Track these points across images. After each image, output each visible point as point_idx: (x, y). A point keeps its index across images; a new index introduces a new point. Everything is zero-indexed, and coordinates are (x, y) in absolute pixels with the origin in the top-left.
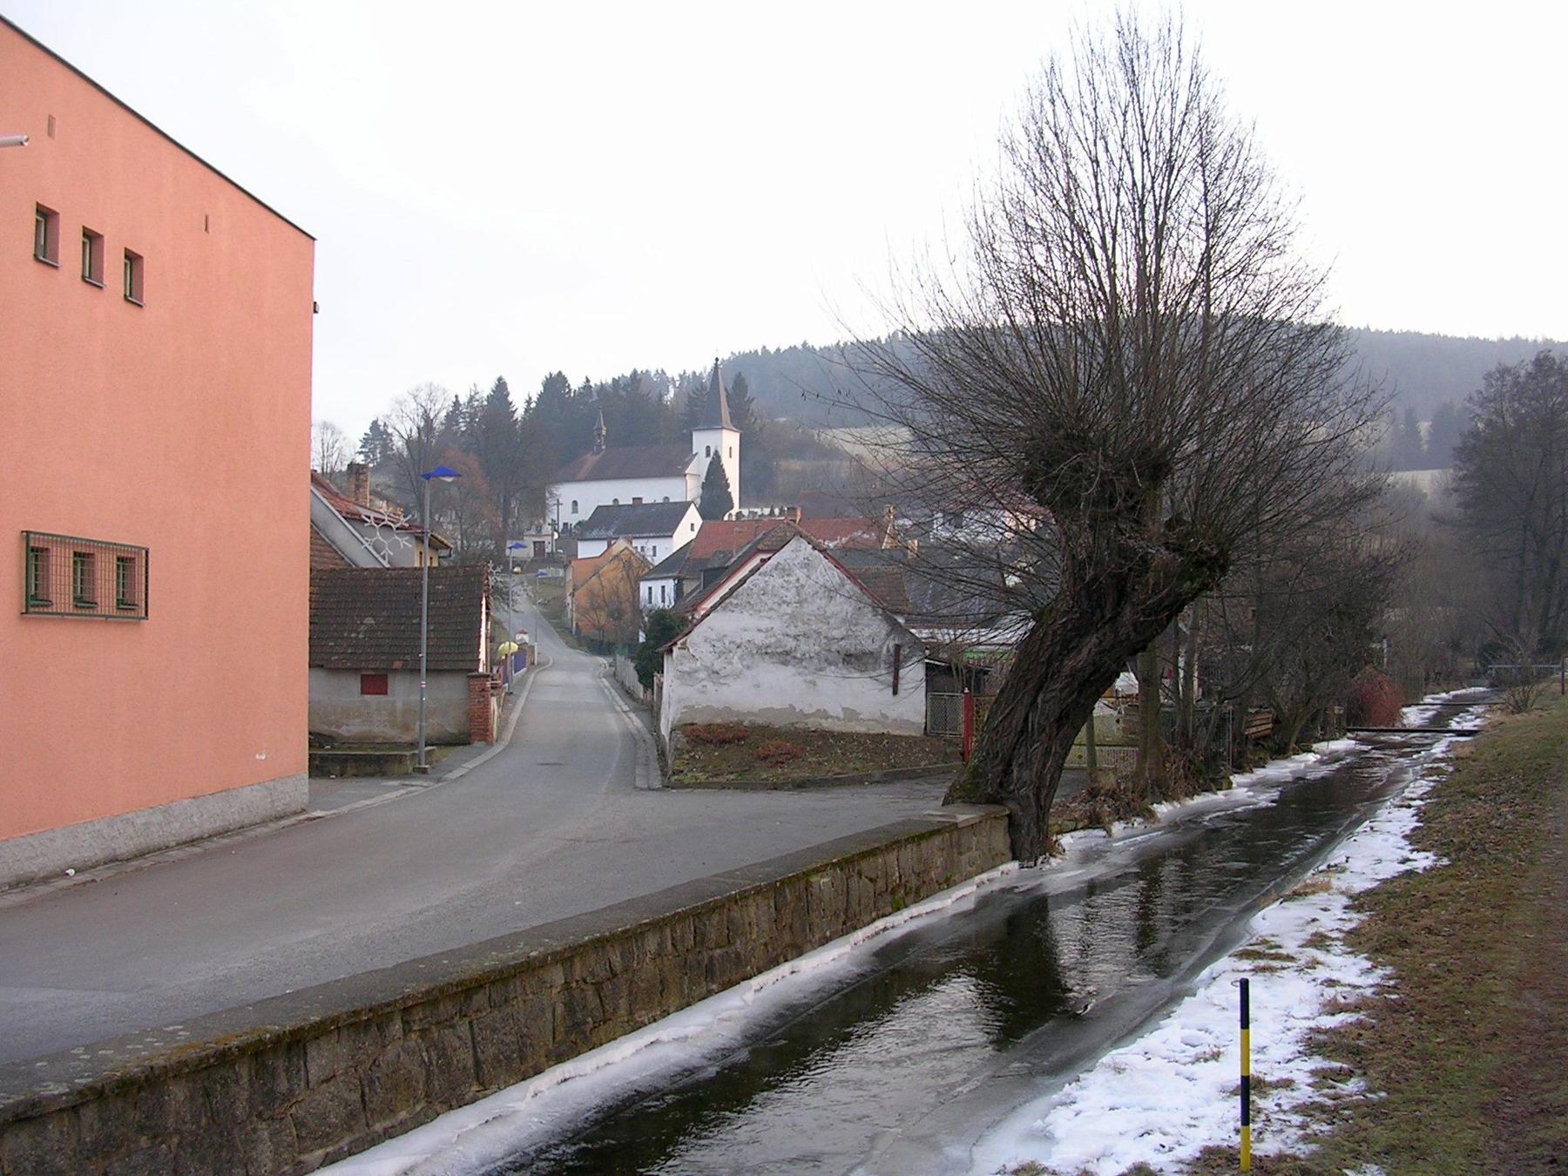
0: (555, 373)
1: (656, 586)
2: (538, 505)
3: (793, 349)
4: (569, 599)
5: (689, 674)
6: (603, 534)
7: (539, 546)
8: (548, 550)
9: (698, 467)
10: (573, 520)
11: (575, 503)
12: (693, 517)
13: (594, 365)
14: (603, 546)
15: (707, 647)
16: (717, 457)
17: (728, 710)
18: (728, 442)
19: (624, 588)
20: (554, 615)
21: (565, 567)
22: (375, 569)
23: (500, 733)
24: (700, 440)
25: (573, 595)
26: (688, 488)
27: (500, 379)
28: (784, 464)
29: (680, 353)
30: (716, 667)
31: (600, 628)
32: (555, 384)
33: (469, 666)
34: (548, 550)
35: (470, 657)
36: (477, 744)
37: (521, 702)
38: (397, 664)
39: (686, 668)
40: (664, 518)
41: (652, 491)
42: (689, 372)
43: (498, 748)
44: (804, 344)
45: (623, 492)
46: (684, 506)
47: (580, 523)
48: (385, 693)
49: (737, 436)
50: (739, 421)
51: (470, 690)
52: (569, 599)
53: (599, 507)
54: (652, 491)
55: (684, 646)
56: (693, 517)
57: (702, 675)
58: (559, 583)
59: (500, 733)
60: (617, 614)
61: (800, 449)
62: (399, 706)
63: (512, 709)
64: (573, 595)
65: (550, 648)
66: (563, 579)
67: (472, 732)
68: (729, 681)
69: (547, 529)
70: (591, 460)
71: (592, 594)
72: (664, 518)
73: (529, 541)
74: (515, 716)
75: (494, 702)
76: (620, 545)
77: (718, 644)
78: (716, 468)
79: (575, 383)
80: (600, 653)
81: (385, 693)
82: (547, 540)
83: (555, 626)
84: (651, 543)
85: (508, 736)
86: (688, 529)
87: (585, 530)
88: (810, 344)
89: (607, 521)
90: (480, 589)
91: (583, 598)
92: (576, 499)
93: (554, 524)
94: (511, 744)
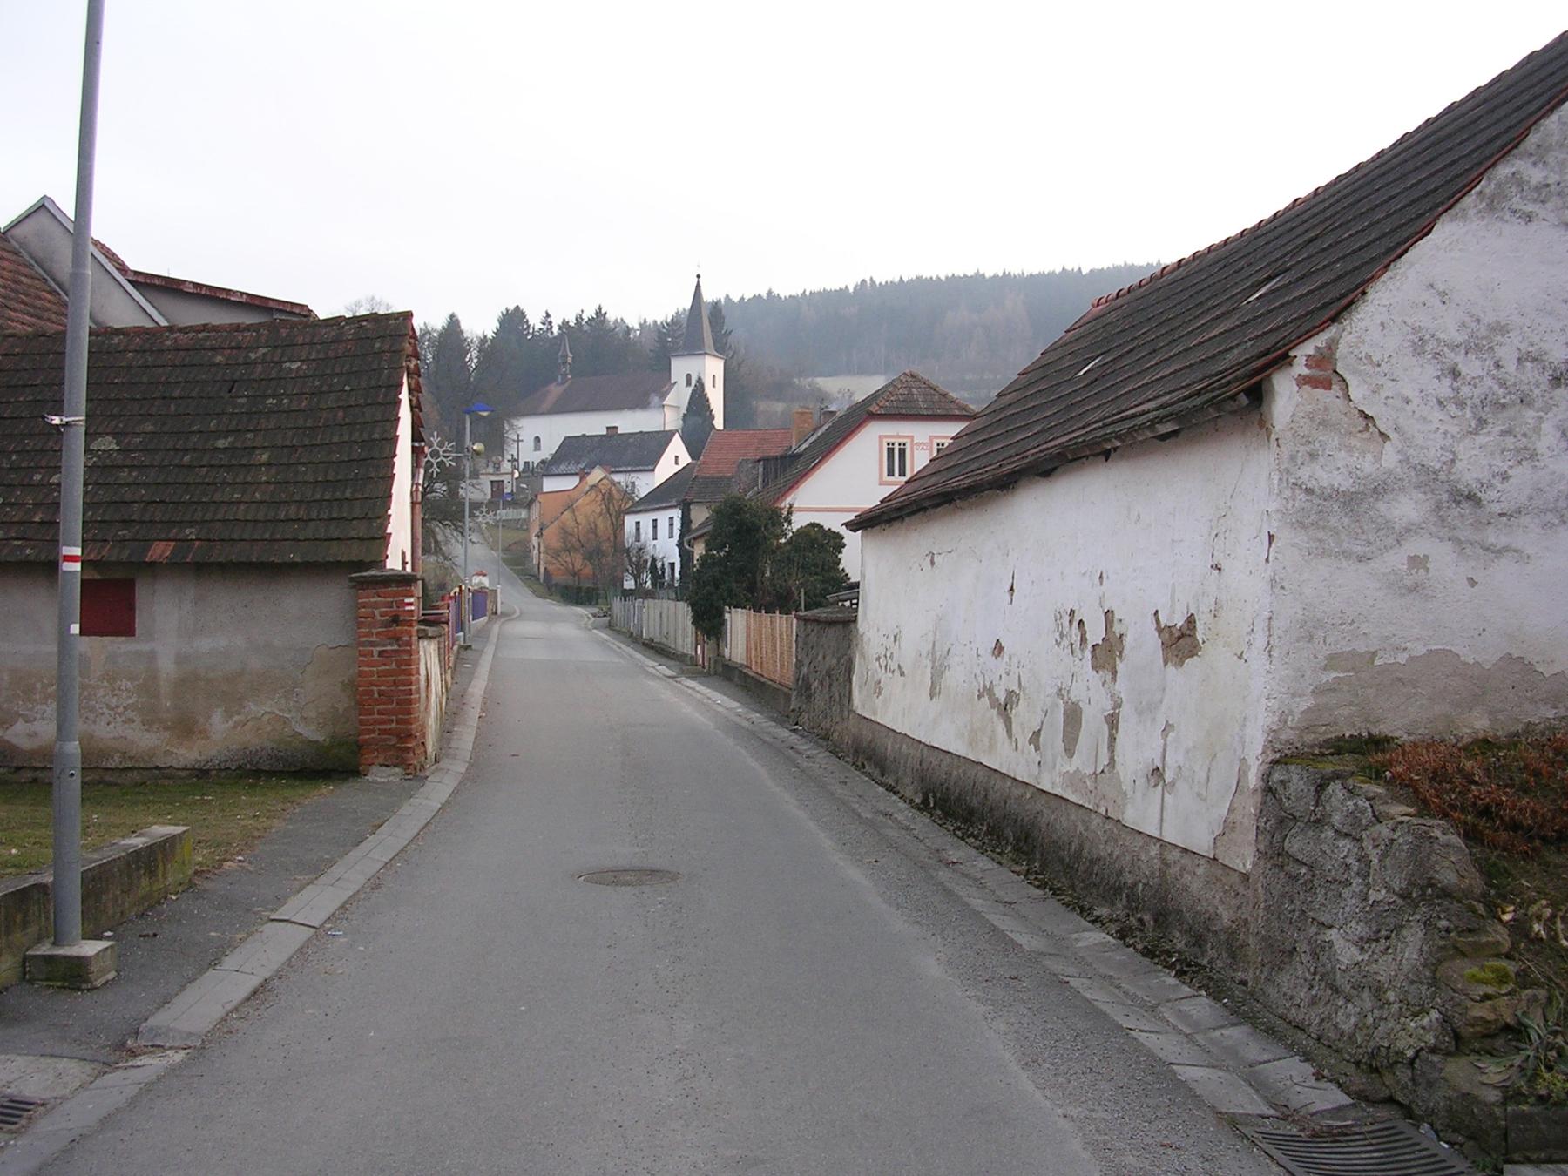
0: (512, 308)
1: (646, 520)
2: (496, 442)
3: (757, 298)
4: (535, 541)
5: (1350, 501)
6: (574, 468)
7: (497, 486)
8: (508, 490)
9: (679, 396)
10: (536, 458)
11: (537, 439)
12: (677, 448)
13: (554, 302)
14: (576, 480)
15: (1420, 378)
16: (700, 382)
17: (1518, 668)
18: (712, 369)
19: (603, 525)
20: (517, 560)
21: (529, 505)
22: (139, 331)
23: (446, 732)
24: (680, 368)
25: (539, 536)
26: (668, 415)
27: (452, 316)
28: (763, 406)
29: (644, 301)
30: (1469, 472)
31: (575, 574)
32: (513, 320)
33: (354, 553)
34: (508, 490)
35: (360, 530)
36: (380, 775)
37: (486, 661)
38: (160, 551)
39: (1332, 473)
40: (648, 449)
41: (630, 422)
42: (650, 321)
43: (437, 790)
44: (770, 292)
45: (593, 424)
46: (666, 437)
47: (543, 462)
48: (128, 630)
49: (721, 364)
50: (721, 348)
51: (360, 621)
52: (535, 541)
53: (567, 438)
54: (630, 422)
55: (1325, 375)
56: (677, 448)
57: (1407, 508)
58: (522, 526)
59: (446, 732)
60: (593, 555)
61: (779, 390)
62: (167, 666)
63: (471, 675)
64: (539, 536)
65: (511, 595)
66: (527, 521)
67: (360, 746)
68: (1526, 536)
69: (506, 466)
70: (555, 390)
71: (565, 533)
72: (648, 449)
73: (485, 482)
74: (478, 688)
75: (428, 657)
76: (597, 475)
77: (1471, 367)
78: (699, 399)
79: (535, 321)
80: (579, 601)
81: (128, 630)
82: (507, 478)
83: (518, 573)
84: (634, 477)
85: (465, 739)
86: (674, 458)
87: (548, 468)
88: (775, 292)
89: (573, 453)
90: (396, 369)
91: (553, 537)
92: (538, 435)
93: (513, 460)
94: (476, 772)
